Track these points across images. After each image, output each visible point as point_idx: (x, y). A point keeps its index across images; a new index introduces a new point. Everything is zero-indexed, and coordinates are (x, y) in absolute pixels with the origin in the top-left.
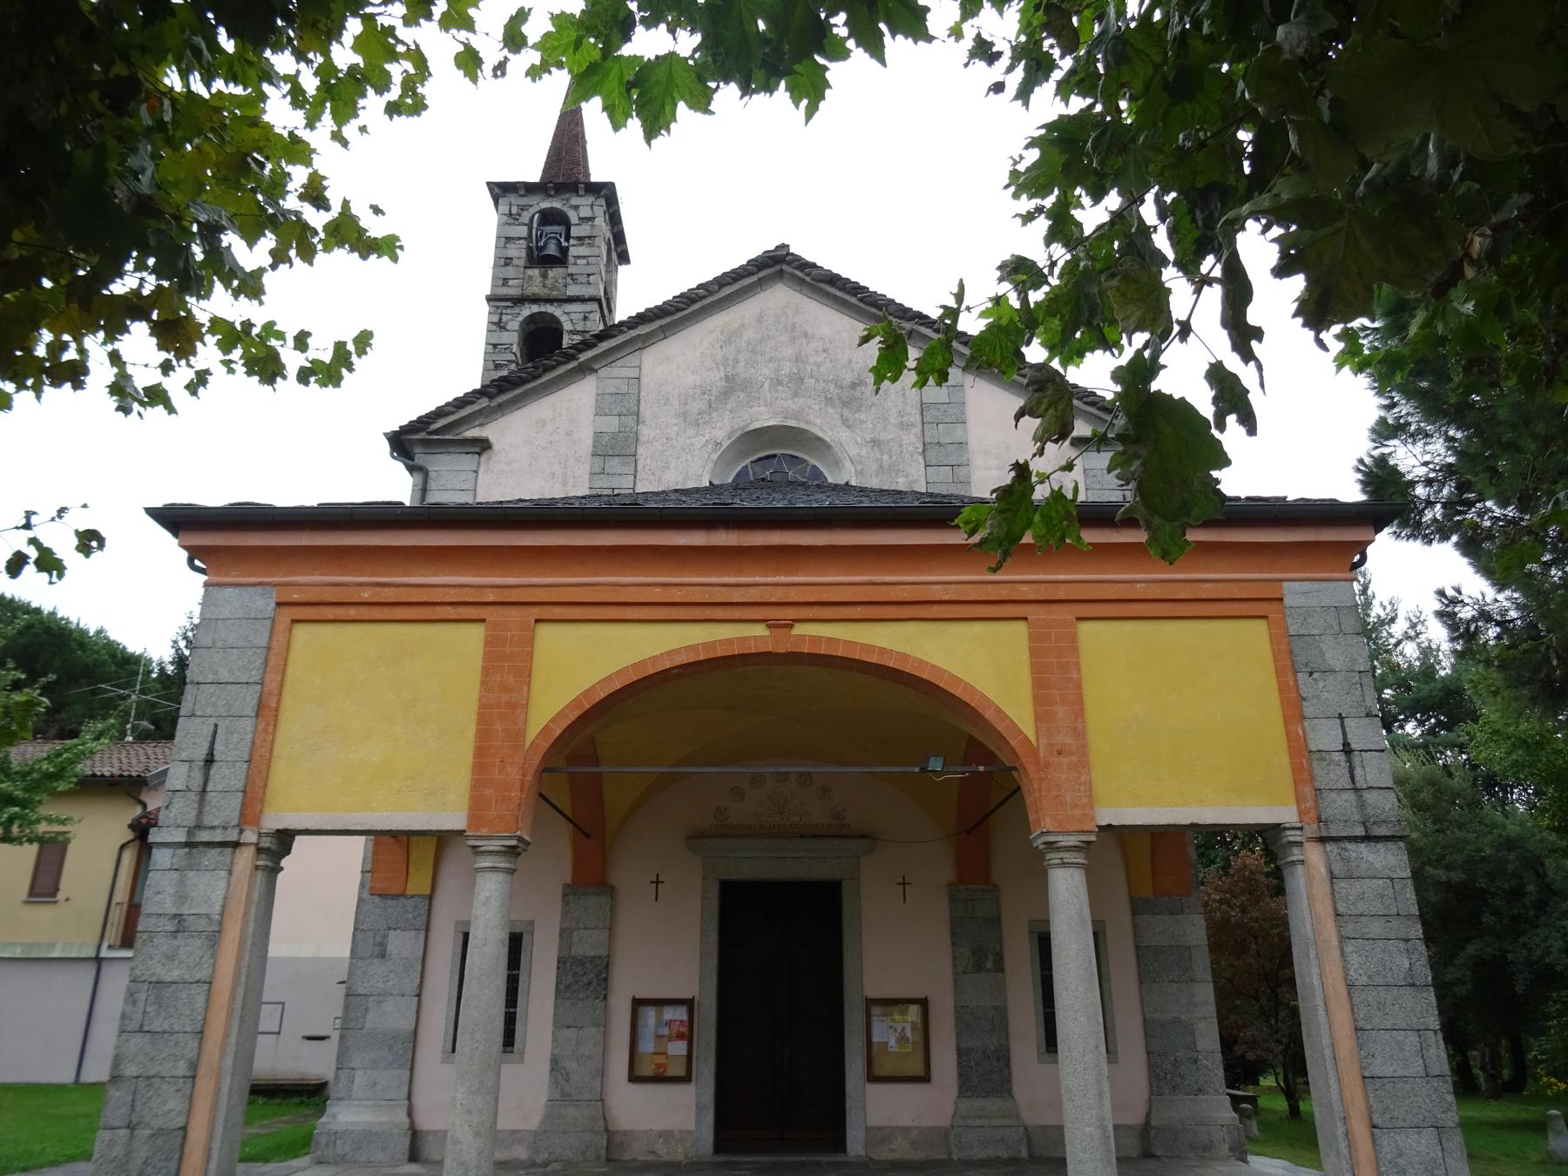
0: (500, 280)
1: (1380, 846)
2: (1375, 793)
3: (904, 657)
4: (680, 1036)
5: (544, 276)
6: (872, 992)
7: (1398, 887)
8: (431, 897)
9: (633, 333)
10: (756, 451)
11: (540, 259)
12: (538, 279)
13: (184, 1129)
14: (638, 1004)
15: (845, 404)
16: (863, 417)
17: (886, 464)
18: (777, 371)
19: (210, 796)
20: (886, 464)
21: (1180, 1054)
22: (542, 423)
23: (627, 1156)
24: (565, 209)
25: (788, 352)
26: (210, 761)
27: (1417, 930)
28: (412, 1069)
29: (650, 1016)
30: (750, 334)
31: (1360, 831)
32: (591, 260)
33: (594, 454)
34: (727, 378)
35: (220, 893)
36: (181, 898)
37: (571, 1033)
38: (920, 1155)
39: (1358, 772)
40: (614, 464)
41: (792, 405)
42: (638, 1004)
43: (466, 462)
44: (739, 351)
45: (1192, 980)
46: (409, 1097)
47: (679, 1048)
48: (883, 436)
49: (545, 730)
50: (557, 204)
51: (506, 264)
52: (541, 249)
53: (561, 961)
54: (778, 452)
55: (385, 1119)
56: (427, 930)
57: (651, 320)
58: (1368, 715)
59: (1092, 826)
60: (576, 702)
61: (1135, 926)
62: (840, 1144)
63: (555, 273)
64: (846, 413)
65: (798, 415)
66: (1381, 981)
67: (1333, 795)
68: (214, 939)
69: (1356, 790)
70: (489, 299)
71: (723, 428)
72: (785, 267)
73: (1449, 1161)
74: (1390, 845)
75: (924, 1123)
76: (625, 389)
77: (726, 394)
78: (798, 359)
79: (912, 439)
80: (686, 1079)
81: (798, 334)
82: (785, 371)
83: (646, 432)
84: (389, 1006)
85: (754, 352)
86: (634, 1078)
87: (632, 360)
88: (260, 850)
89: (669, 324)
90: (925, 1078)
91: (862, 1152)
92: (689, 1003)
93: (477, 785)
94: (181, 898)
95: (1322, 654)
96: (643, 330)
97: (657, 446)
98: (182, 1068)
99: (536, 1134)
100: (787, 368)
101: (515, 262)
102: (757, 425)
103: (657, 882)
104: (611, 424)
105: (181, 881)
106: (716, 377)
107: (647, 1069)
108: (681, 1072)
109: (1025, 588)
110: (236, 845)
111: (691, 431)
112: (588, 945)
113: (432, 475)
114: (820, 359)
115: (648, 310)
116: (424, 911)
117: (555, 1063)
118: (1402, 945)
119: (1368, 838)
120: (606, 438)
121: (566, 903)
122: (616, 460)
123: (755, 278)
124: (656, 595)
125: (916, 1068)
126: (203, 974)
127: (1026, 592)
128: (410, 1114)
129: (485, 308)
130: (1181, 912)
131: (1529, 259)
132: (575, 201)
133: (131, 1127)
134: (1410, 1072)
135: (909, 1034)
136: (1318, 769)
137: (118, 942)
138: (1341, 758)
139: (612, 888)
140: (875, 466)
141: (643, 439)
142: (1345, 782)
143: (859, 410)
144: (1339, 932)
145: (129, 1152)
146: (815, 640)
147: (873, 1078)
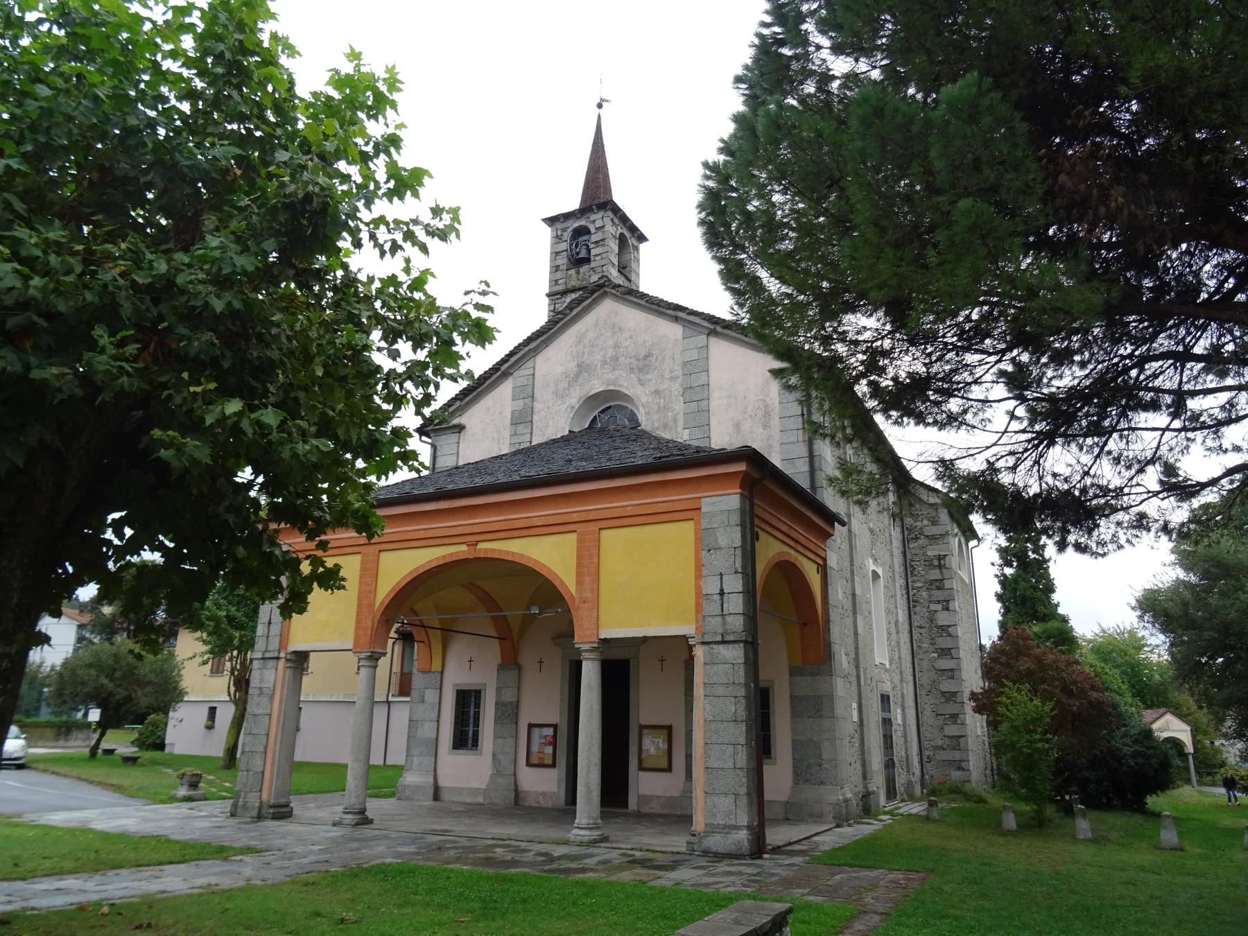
0: (554, 282)
1: (730, 646)
2: (732, 617)
3: (522, 556)
4: (550, 744)
5: (578, 273)
6: (643, 722)
7: (736, 668)
8: (442, 673)
9: (527, 349)
10: (599, 406)
11: (578, 261)
12: (574, 276)
13: (263, 772)
14: (531, 726)
15: (641, 370)
16: (650, 377)
17: (662, 405)
18: (604, 356)
19: (270, 638)
20: (662, 405)
21: (811, 761)
22: (488, 409)
23: (527, 804)
24: (587, 224)
25: (611, 342)
26: (270, 623)
27: (742, 692)
28: (436, 757)
29: (536, 731)
30: (591, 335)
31: (719, 638)
32: (604, 255)
33: (512, 424)
34: (579, 366)
35: (273, 679)
36: (261, 681)
37: (500, 741)
38: (666, 811)
39: (725, 605)
40: (521, 429)
41: (611, 376)
42: (531, 726)
43: (453, 438)
44: (585, 347)
45: (822, 716)
46: (435, 770)
47: (549, 750)
48: (662, 387)
49: (383, 602)
50: (582, 222)
51: (557, 271)
52: (578, 254)
53: (497, 704)
54: (612, 404)
55: (424, 780)
56: (441, 689)
57: (536, 339)
58: (736, 572)
59: (595, 639)
60: (393, 589)
61: (791, 684)
62: (625, 805)
63: (584, 269)
64: (641, 376)
65: (615, 382)
66: (719, 719)
67: (710, 619)
68: (272, 697)
69: (723, 615)
70: (548, 295)
71: (576, 397)
72: (606, 289)
73: (738, 811)
74: (736, 645)
75: (668, 794)
76: (526, 383)
77: (578, 375)
78: (616, 346)
79: (676, 387)
80: (553, 765)
81: (616, 329)
82: (609, 355)
83: (537, 406)
84: (426, 726)
85: (592, 346)
86: (529, 764)
87: (530, 364)
88: (288, 660)
89: (548, 339)
90: (669, 769)
91: (636, 808)
92: (555, 727)
93: (357, 629)
94: (261, 681)
95: (717, 539)
96: (532, 346)
97: (543, 413)
98: (262, 749)
99: (485, 790)
100: (610, 352)
101: (561, 268)
102: (593, 392)
103: (541, 662)
104: (520, 404)
105: (262, 673)
106: (572, 366)
107: (535, 760)
108: (664, 765)
109: (574, 515)
110: (278, 658)
111: (559, 402)
112: (509, 696)
113: (438, 447)
114: (628, 343)
115: (533, 334)
116: (439, 679)
117: (494, 755)
118: (733, 700)
119: (723, 642)
120: (517, 413)
121: (499, 674)
122: (522, 426)
123: (590, 300)
124: (422, 535)
125: (664, 765)
126: (268, 711)
127: (576, 517)
128: (435, 778)
129: (547, 299)
130: (819, 674)
131: (156, 557)
132: (593, 217)
133: (247, 771)
134: (726, 766)
135: (661, 745)
136: (705, 605)
137: (397, 693)
138: (718, 597)
139: (520, 666)
140: (656, 408)
141: (536, 410)
142: (718, 611)
143: (648, 373)
144: (792, 690)
145: (247, 779)
146: (486, 550)
147: (641, 768)
